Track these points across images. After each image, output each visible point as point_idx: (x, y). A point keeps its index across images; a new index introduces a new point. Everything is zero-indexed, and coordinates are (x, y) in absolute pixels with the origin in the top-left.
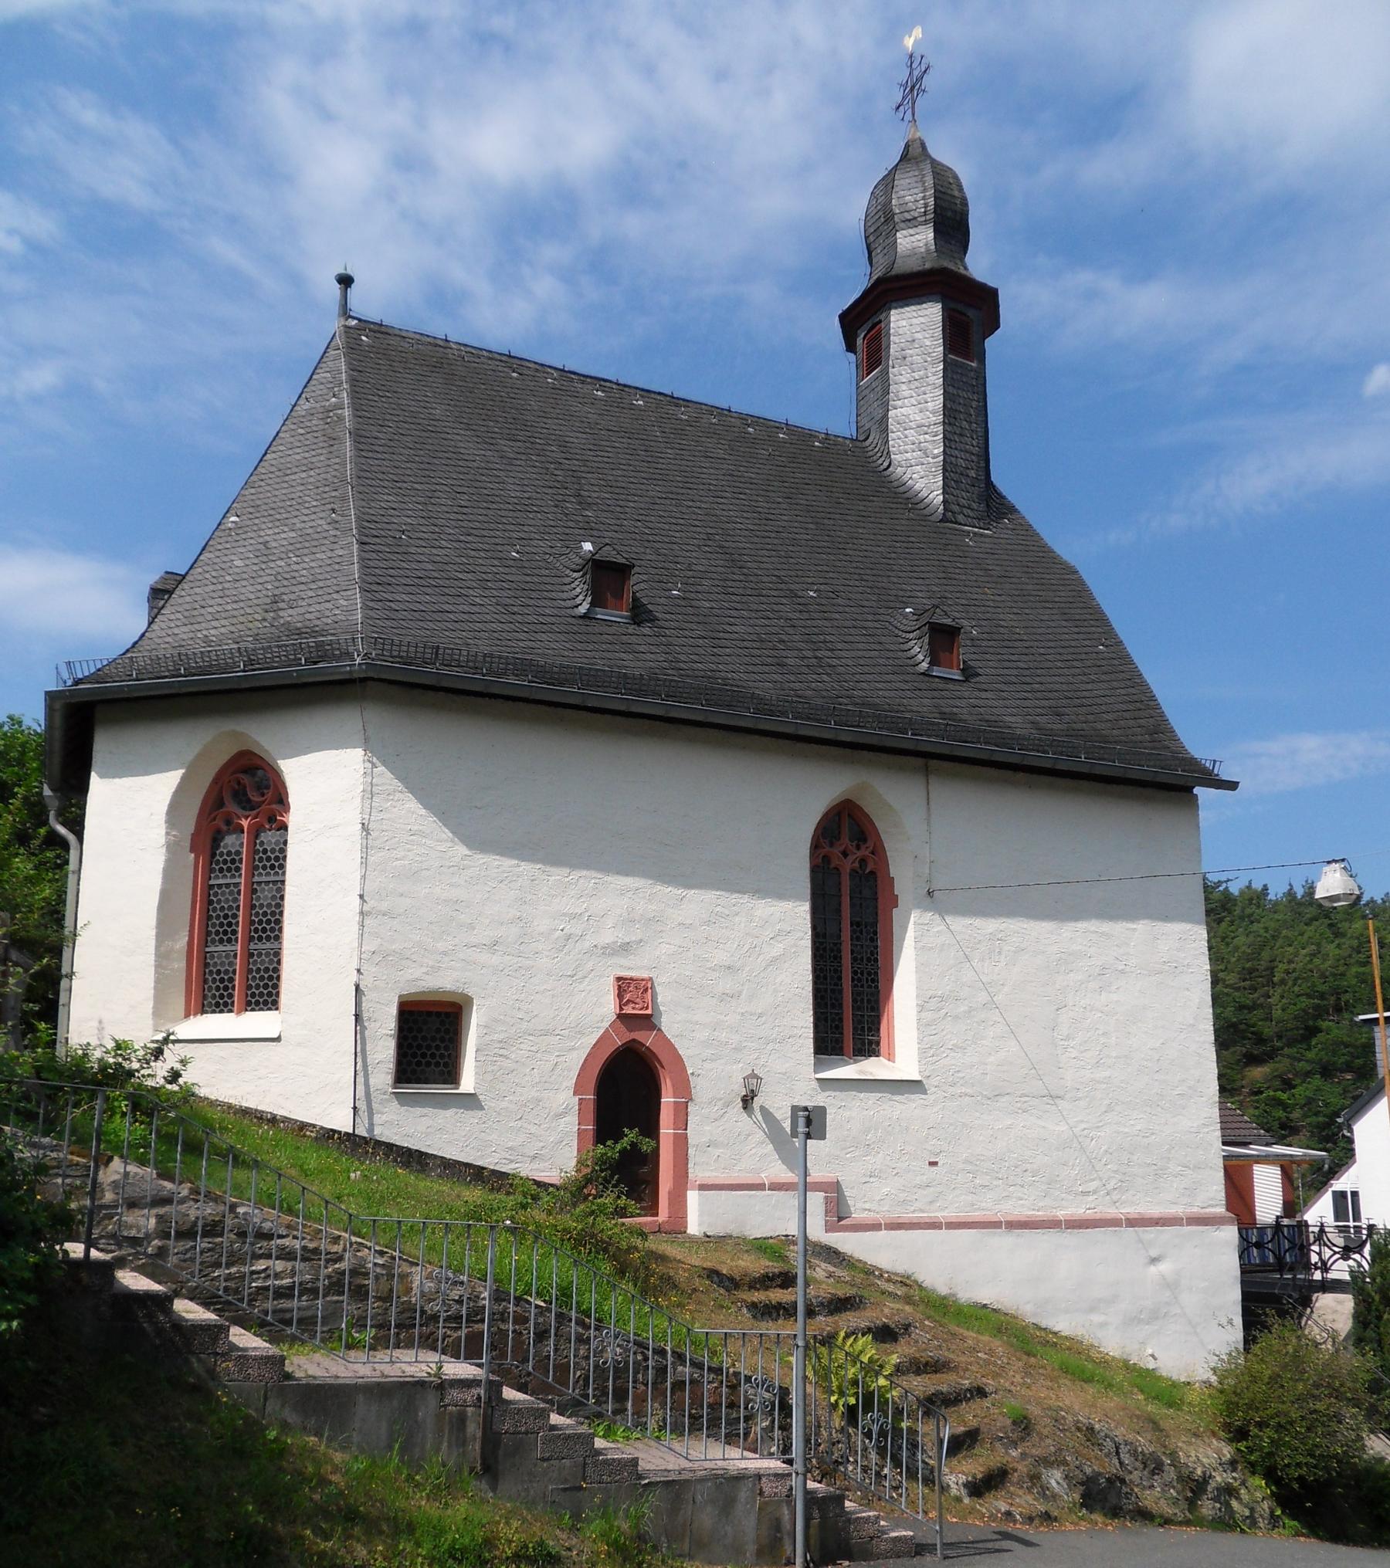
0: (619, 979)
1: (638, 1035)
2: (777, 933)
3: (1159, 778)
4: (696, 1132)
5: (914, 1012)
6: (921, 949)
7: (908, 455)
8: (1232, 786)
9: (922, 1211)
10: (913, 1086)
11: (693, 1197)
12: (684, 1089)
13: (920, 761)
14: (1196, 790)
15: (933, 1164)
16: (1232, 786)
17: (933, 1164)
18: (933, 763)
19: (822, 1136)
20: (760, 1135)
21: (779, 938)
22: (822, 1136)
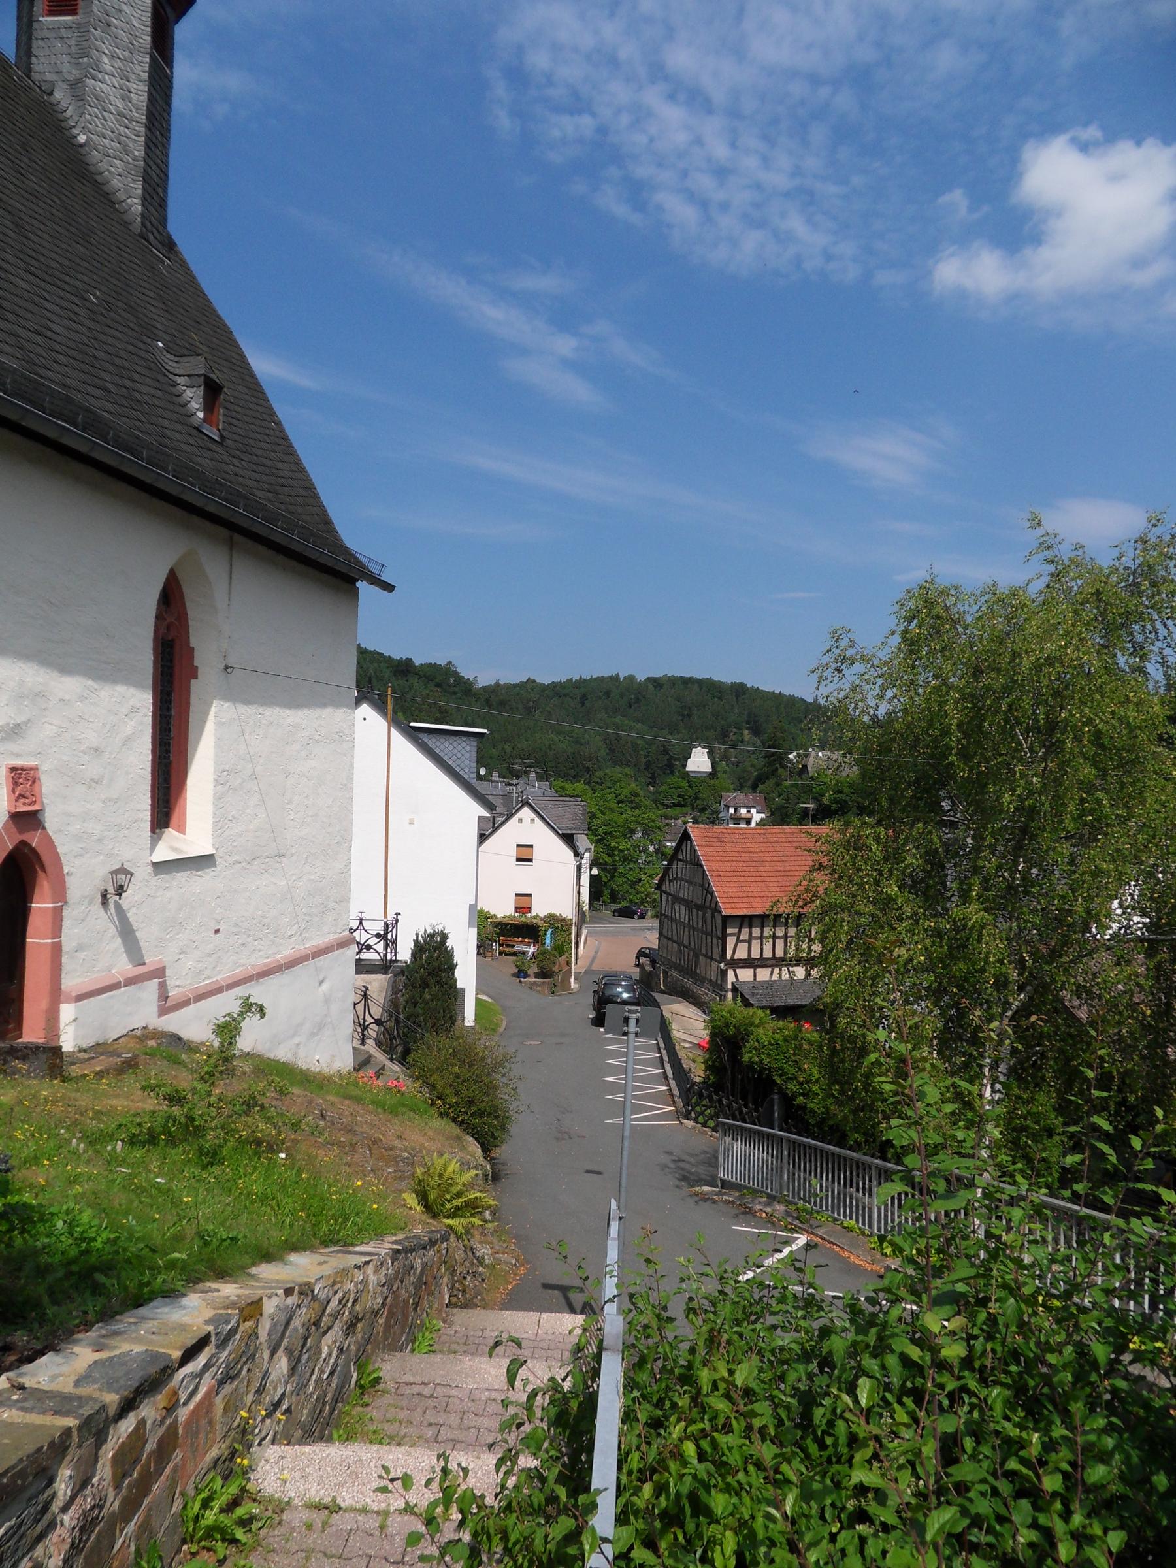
0: (13, 769)
1: (26, 837)
2: (125, 711)
3: (335, 572)
4: (69, 940)
5: (211, 786)
6: (219, 724)
7: (106, 142)
8: (389, 588)
9: (209, 978)
10: (206, 861)
11: (67, 1011)
12: (60, 894)
13: (224, 532)
14: (358, 584)
15: (217, 931)
16: (389, 588)
17: (217, 931)
18: (237, 537)
19: (471, 905)
20: (112, 931)
21: (132, 715)
22: (471, 905)
